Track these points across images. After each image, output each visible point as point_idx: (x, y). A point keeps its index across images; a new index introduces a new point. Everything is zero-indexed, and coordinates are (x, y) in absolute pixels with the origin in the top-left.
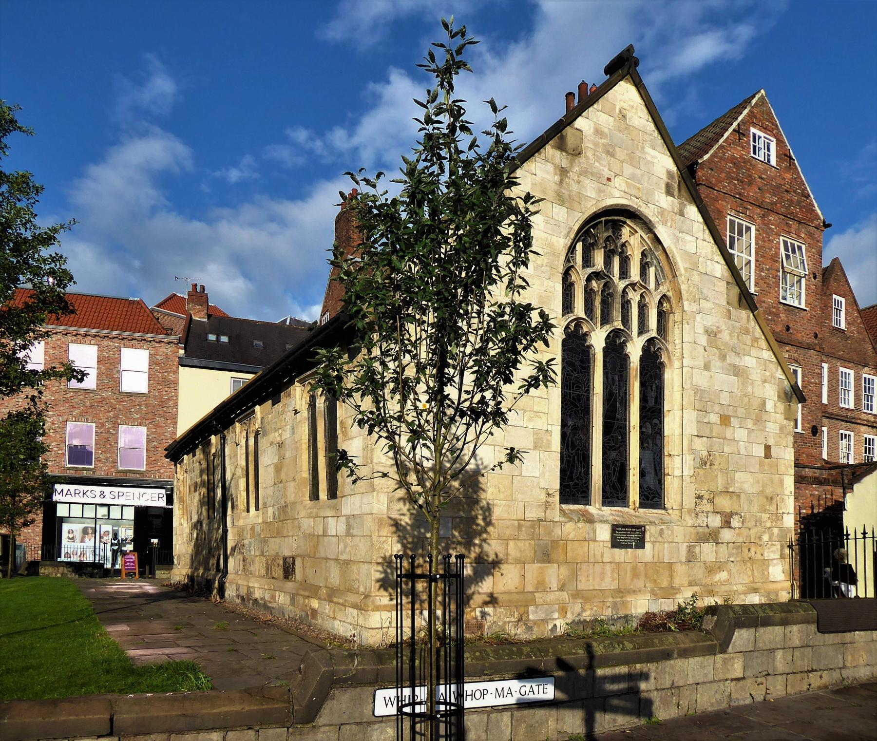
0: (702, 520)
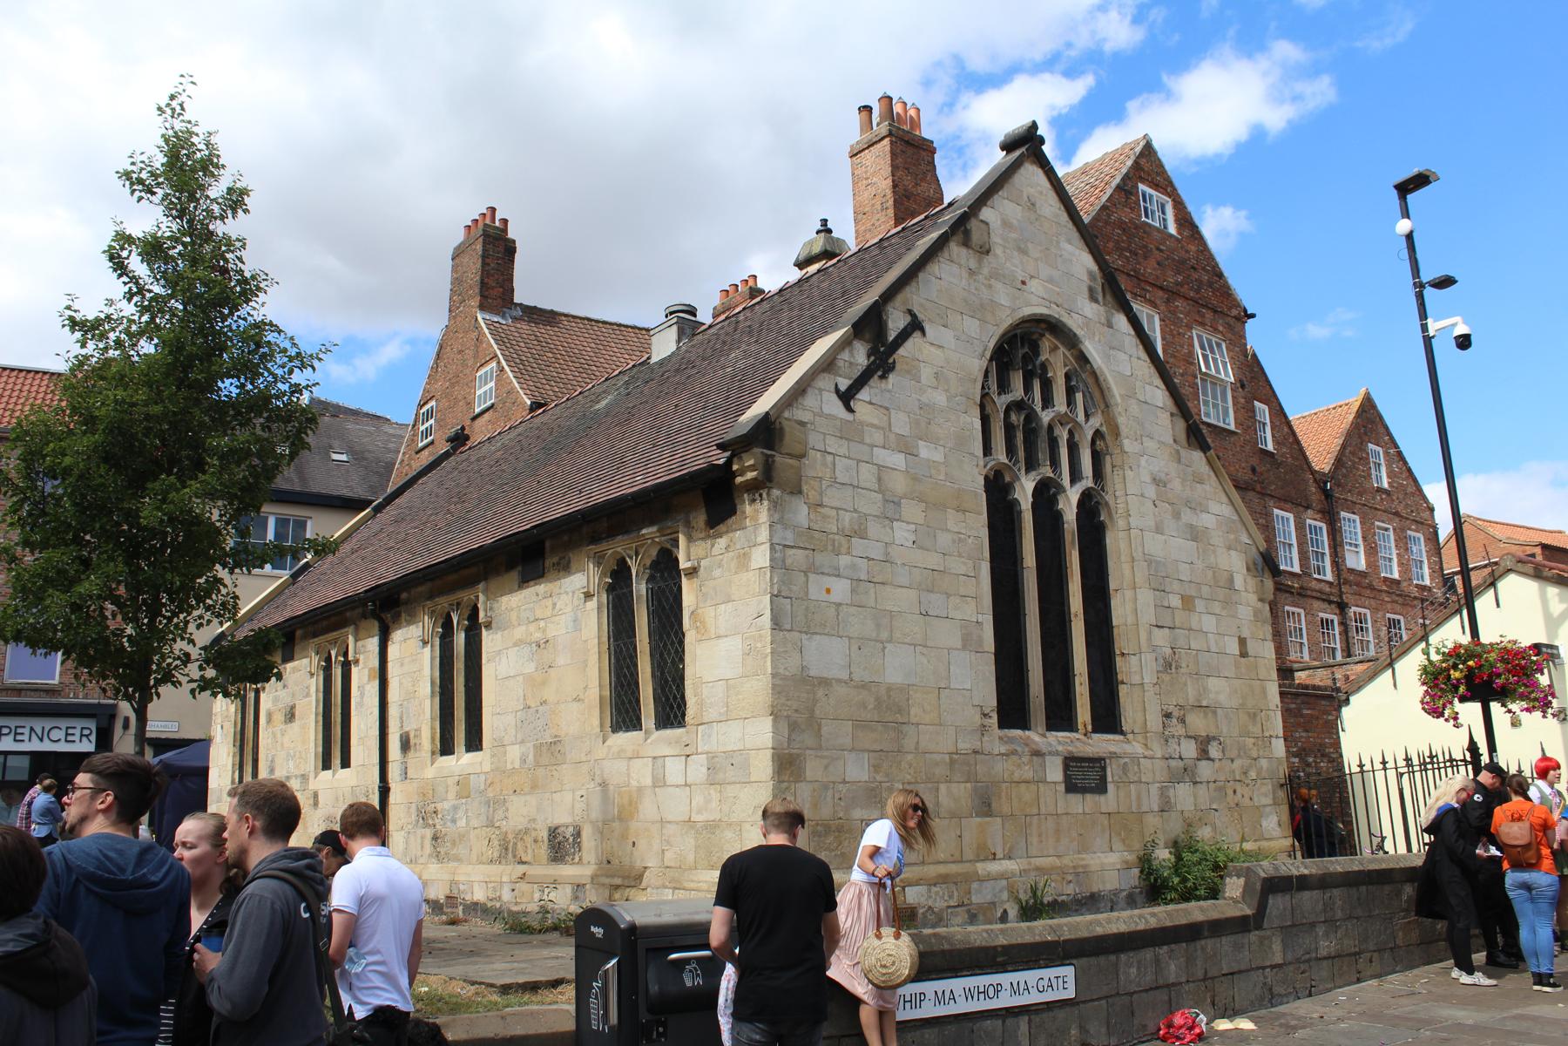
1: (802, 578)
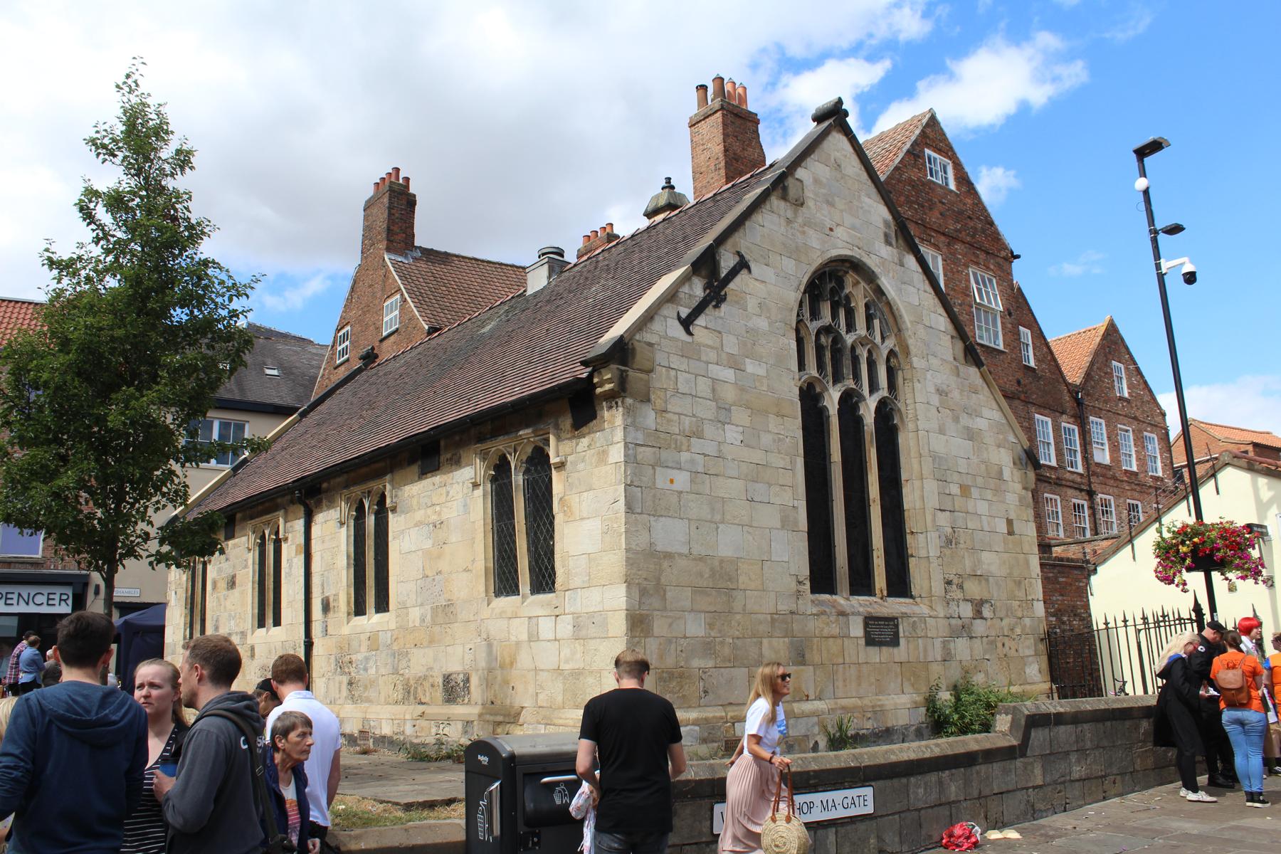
0: (953, 609)
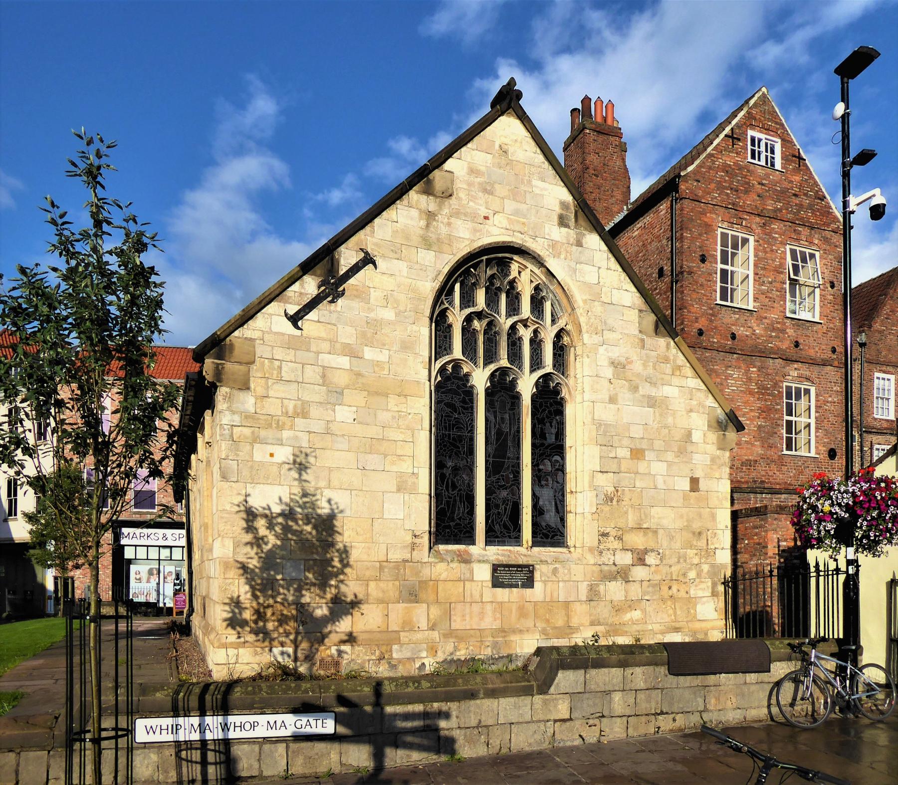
0: (607, 558)
1: (248, 447)
